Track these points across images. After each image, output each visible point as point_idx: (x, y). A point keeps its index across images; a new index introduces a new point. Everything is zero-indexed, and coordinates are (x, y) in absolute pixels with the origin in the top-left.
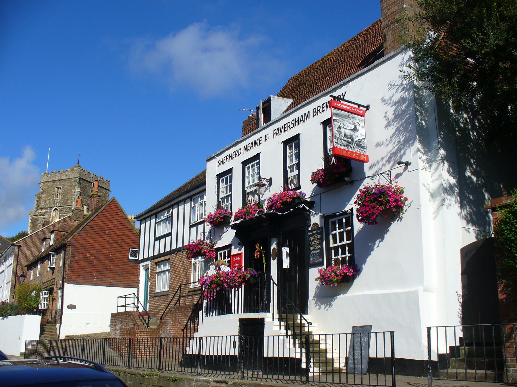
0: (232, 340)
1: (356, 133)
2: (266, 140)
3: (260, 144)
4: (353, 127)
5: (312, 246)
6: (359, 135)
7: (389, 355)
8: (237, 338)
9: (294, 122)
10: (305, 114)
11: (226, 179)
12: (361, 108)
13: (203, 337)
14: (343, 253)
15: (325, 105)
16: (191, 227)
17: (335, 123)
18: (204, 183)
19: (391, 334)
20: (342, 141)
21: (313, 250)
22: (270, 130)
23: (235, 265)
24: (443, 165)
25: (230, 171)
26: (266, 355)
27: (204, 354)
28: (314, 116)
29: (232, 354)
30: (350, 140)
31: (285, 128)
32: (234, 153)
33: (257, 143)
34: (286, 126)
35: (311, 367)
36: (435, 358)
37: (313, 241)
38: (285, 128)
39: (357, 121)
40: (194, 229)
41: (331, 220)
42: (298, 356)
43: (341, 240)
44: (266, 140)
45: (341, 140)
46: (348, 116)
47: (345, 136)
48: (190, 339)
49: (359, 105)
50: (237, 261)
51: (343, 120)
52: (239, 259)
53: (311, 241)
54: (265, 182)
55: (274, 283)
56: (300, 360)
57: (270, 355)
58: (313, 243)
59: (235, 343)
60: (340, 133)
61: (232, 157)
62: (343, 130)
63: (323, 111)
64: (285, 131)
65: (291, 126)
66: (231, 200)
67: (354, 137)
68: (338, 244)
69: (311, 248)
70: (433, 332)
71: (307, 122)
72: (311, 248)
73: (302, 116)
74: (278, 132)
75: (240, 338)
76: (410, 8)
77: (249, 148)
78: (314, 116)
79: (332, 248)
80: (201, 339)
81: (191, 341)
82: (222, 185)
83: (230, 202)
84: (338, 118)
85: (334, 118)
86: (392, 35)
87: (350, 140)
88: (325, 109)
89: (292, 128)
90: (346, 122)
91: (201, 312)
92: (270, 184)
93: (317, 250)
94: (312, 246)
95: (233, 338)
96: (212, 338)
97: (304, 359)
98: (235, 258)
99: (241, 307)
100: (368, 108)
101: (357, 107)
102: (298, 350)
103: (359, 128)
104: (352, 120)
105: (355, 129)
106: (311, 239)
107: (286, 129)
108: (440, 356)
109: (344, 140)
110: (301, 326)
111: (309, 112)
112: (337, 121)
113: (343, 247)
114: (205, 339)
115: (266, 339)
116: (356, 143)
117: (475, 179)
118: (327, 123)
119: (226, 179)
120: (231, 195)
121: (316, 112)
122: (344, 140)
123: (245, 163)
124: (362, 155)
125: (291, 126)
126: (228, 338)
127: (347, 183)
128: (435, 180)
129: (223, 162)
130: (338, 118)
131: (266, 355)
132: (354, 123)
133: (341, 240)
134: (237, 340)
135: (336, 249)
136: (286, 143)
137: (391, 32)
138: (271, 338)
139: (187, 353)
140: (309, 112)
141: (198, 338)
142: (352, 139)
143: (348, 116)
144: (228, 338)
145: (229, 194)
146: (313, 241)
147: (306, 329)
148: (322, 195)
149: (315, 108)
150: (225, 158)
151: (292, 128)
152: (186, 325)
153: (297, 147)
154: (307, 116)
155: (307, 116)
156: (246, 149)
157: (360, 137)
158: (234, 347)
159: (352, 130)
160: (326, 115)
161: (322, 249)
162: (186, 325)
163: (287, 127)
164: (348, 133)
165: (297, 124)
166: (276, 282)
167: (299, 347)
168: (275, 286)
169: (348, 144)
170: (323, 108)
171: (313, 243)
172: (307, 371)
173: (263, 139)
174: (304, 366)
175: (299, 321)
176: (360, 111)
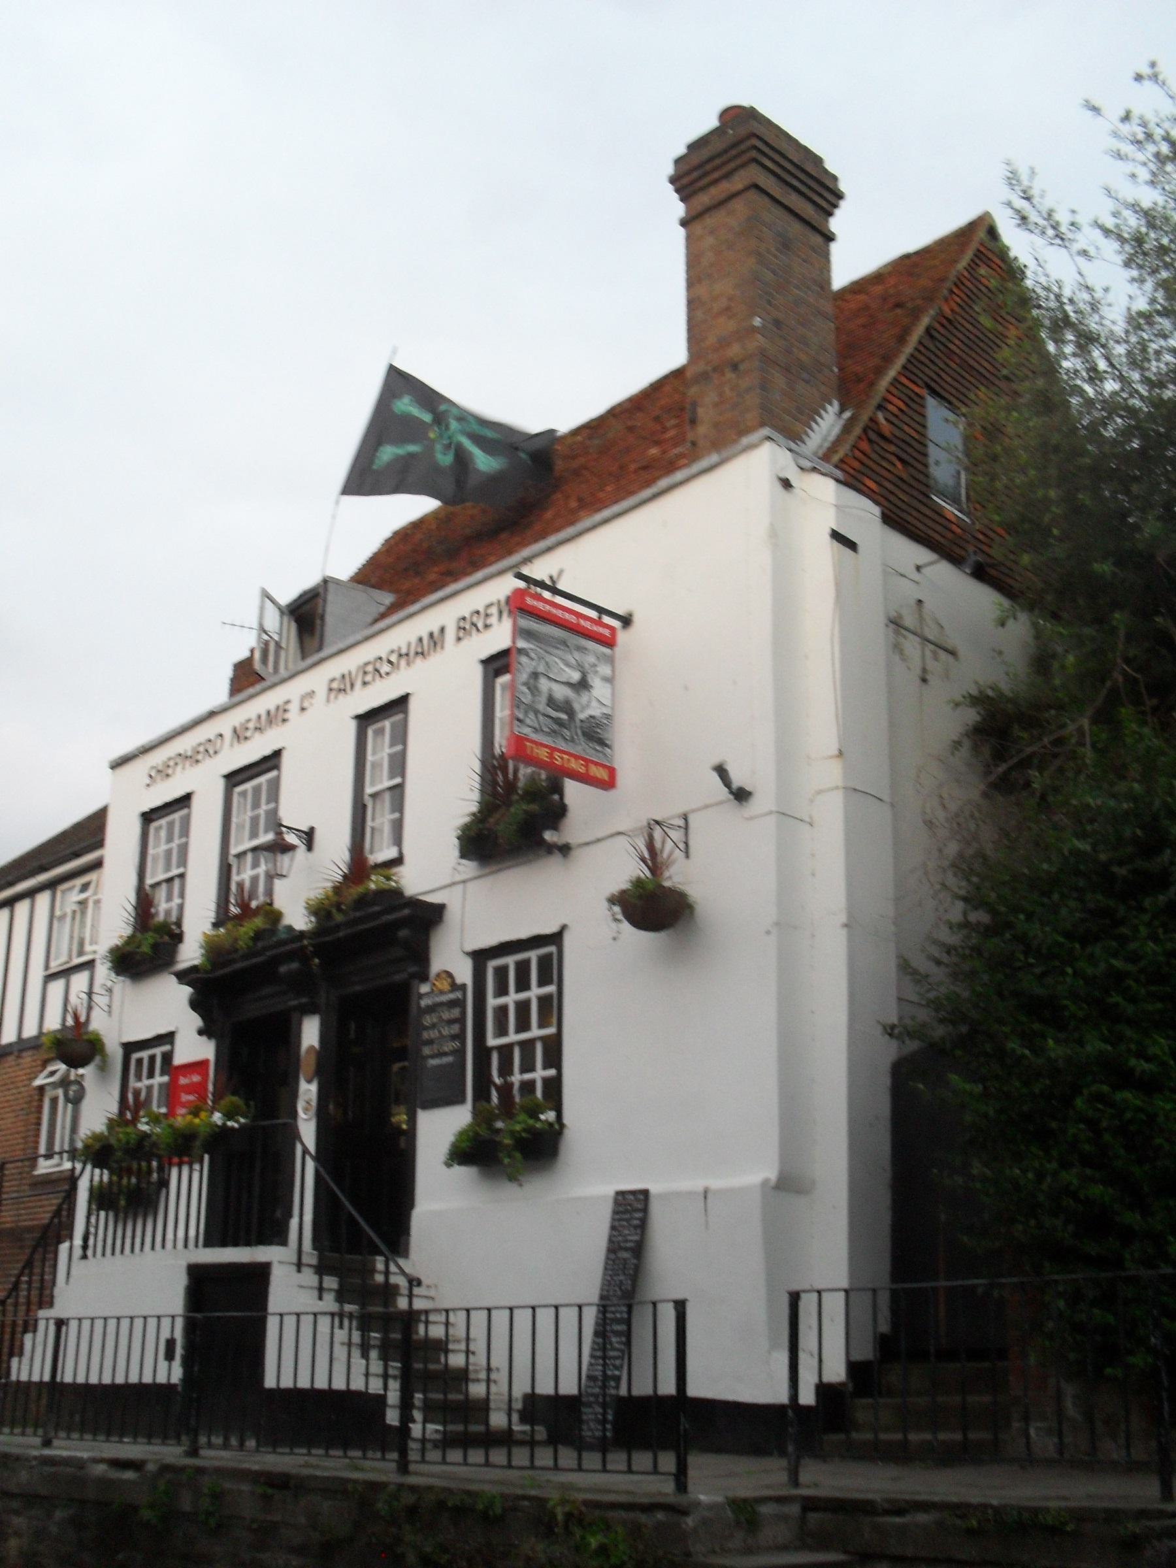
0: (165, 1334)
1: (585, 697)
2: (303, 709)
3: (284, 720)
4: (576, 676)
5: (430, 1042)
6: (594, 704)
7: (668, 1387)
8: (179, 1323)
9: (393, 658)
10: (431, 635)
11: (171, 825)
12: (607, 620)
13: (68, 1319)
14: (528, 1067)
15: (494, 610)
16: (50, 978)
17: (524, 659)
18: (100, 844)
19: (676, 1309)
20: (537, 717)
21: (432, 1057)
22: (317, 679)
23: (185, 1098)
24: (904, 660)
25: (185, 800)
26: (270, 1382)
27: (68, 1379)
28: (459, 639)
29: (162, 1379)
30: (564, 716)
31: (365, 673)
32: (201, 749)
33: (276, 717)
34: (370, 668)
35: (414, 1421)
36: (807, 1397)
37: (434, 1026)
38: (365, 673)
39: (591, 659)
40: (57, 987)
41: (492, 965)
42: (375, 1386)
43: (523, 1025)
44: (303, 709)
45: (536, 712)
46: (565, 643)
47: (551, 702)
48: (25, 1331)
49: (601, 610)
50: (193, 1084)
51: (546, 651)
52: (196, 1078)
53: (426, 1028)
54: (291, 839)
55: (305, 1151)
56: (381, 1400)
57: (287, 1383)
58: (434, 1034)
59: (171, 1343)
60: (534, 690)
61: (192, 758)
62: (544, 684)
63: (487, 626)
64: (365, 683)
65: (385, 668)
66: (182, 895)
67: (576, 706)
68: (513, 1037)
69: (426, 1051)
70: (808, 1304)
71: (436, 660)
72: (426, 1051)
73: (421, 640)
74: (342, 686)
75: (191, 1326)
76: (775, 329)
77: (248, 734)
78: (459, 639)
79: (493, 1048)
80: (60, 1323)
81: (28, 1338)
82: (157, 850)
83: (177, 901)
84: (532, 646)
85: (521, 644)
86: (716, 405)
87: (564, 716)
88: (493, 620)
89: (387, 674)
90: (556, 660)
91: (64, 1247)
92: (310, 847)
93: (445, 1054)
94: (430, 1042)
95: (166, 1323)
96: (99, 1324)
97: (393, 1397)
98: (185, 1076)
99: (196, 1225)
100: (626, 621)
101: (593, 614)
102: (376, 1366)
103: (596, 682)
104: (577, 655)
105: (583, 685)
106: (428, 1020)
107: (368, 678)
108: (824, 1390)
109: (544, 715)
110: (389, 1291)
111: (442, 630)
112: (527, 655)
113: (527, 1047)
114: (73, 1325)
115: (272, 1324)
116: (581, 727)
117: (311, 1033)
118: (497, 664)
119: (171, 825)
120: (182, 876)
121: (467, 627)
122: (544, 715)
123: (234, 778)
124: (596, 764)
125: (385, 668)
126: (152, 1323)
127: (551, 849)
128: (1078, 268)
129: (163, 773)
130: (532, 646)
131: (270, 1382)
132: (580, 667)
133: (523, 1025)
134: (179, 1335)
135: (506, 1052)
136: (366, 719)
137: (711, 397)
138: (290, 1322)
139: (14, 1377)
140: (442, 630)
141: (52, 1322)
142: (571, 713)
143: (565, 643)
144: (152, 1323)
145: (175, 872)
146: (434, 1026)
147: (402, 1303)
148: (470, 885)
149: (464, 619)
150: (171, 763)
151: (387, 674)
152: (16, 1287)
153: (401, 736)
154: (436, 640)
155: (436, 640)
156: (239, 735)
157: (595, 711)
158: (169, 1356)
159: (575, 685)
160: (499, 637)
161: (461, 1052)
162: (16, 1287)
163: (374, 671)
164: (561, 692)
165: (403, 662)
166: (311, 1145)
167: (380, 1358)
168: (308, 1158)
169: (556, 727)
170: (487, 615)
171: (434, 1034)
172: (403, 1431)
173: (294, 708)
174: (392, 1417)
175: (379, 1278)
176: (601, 630)
